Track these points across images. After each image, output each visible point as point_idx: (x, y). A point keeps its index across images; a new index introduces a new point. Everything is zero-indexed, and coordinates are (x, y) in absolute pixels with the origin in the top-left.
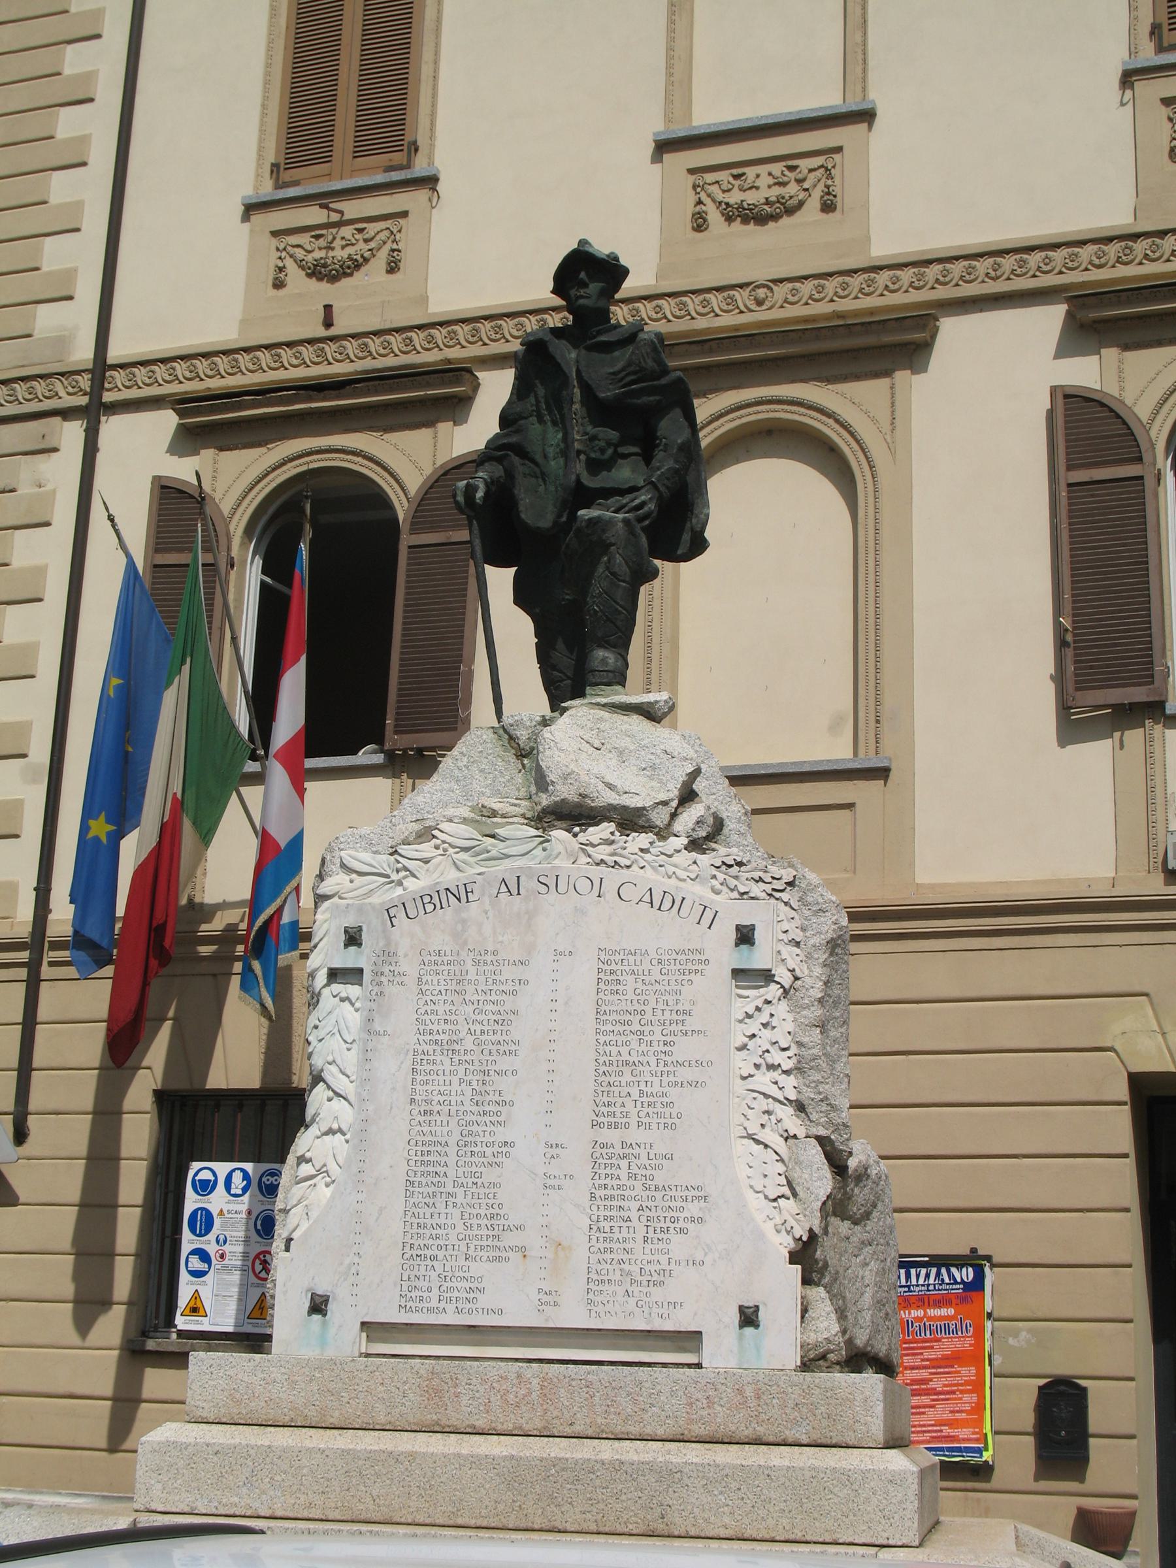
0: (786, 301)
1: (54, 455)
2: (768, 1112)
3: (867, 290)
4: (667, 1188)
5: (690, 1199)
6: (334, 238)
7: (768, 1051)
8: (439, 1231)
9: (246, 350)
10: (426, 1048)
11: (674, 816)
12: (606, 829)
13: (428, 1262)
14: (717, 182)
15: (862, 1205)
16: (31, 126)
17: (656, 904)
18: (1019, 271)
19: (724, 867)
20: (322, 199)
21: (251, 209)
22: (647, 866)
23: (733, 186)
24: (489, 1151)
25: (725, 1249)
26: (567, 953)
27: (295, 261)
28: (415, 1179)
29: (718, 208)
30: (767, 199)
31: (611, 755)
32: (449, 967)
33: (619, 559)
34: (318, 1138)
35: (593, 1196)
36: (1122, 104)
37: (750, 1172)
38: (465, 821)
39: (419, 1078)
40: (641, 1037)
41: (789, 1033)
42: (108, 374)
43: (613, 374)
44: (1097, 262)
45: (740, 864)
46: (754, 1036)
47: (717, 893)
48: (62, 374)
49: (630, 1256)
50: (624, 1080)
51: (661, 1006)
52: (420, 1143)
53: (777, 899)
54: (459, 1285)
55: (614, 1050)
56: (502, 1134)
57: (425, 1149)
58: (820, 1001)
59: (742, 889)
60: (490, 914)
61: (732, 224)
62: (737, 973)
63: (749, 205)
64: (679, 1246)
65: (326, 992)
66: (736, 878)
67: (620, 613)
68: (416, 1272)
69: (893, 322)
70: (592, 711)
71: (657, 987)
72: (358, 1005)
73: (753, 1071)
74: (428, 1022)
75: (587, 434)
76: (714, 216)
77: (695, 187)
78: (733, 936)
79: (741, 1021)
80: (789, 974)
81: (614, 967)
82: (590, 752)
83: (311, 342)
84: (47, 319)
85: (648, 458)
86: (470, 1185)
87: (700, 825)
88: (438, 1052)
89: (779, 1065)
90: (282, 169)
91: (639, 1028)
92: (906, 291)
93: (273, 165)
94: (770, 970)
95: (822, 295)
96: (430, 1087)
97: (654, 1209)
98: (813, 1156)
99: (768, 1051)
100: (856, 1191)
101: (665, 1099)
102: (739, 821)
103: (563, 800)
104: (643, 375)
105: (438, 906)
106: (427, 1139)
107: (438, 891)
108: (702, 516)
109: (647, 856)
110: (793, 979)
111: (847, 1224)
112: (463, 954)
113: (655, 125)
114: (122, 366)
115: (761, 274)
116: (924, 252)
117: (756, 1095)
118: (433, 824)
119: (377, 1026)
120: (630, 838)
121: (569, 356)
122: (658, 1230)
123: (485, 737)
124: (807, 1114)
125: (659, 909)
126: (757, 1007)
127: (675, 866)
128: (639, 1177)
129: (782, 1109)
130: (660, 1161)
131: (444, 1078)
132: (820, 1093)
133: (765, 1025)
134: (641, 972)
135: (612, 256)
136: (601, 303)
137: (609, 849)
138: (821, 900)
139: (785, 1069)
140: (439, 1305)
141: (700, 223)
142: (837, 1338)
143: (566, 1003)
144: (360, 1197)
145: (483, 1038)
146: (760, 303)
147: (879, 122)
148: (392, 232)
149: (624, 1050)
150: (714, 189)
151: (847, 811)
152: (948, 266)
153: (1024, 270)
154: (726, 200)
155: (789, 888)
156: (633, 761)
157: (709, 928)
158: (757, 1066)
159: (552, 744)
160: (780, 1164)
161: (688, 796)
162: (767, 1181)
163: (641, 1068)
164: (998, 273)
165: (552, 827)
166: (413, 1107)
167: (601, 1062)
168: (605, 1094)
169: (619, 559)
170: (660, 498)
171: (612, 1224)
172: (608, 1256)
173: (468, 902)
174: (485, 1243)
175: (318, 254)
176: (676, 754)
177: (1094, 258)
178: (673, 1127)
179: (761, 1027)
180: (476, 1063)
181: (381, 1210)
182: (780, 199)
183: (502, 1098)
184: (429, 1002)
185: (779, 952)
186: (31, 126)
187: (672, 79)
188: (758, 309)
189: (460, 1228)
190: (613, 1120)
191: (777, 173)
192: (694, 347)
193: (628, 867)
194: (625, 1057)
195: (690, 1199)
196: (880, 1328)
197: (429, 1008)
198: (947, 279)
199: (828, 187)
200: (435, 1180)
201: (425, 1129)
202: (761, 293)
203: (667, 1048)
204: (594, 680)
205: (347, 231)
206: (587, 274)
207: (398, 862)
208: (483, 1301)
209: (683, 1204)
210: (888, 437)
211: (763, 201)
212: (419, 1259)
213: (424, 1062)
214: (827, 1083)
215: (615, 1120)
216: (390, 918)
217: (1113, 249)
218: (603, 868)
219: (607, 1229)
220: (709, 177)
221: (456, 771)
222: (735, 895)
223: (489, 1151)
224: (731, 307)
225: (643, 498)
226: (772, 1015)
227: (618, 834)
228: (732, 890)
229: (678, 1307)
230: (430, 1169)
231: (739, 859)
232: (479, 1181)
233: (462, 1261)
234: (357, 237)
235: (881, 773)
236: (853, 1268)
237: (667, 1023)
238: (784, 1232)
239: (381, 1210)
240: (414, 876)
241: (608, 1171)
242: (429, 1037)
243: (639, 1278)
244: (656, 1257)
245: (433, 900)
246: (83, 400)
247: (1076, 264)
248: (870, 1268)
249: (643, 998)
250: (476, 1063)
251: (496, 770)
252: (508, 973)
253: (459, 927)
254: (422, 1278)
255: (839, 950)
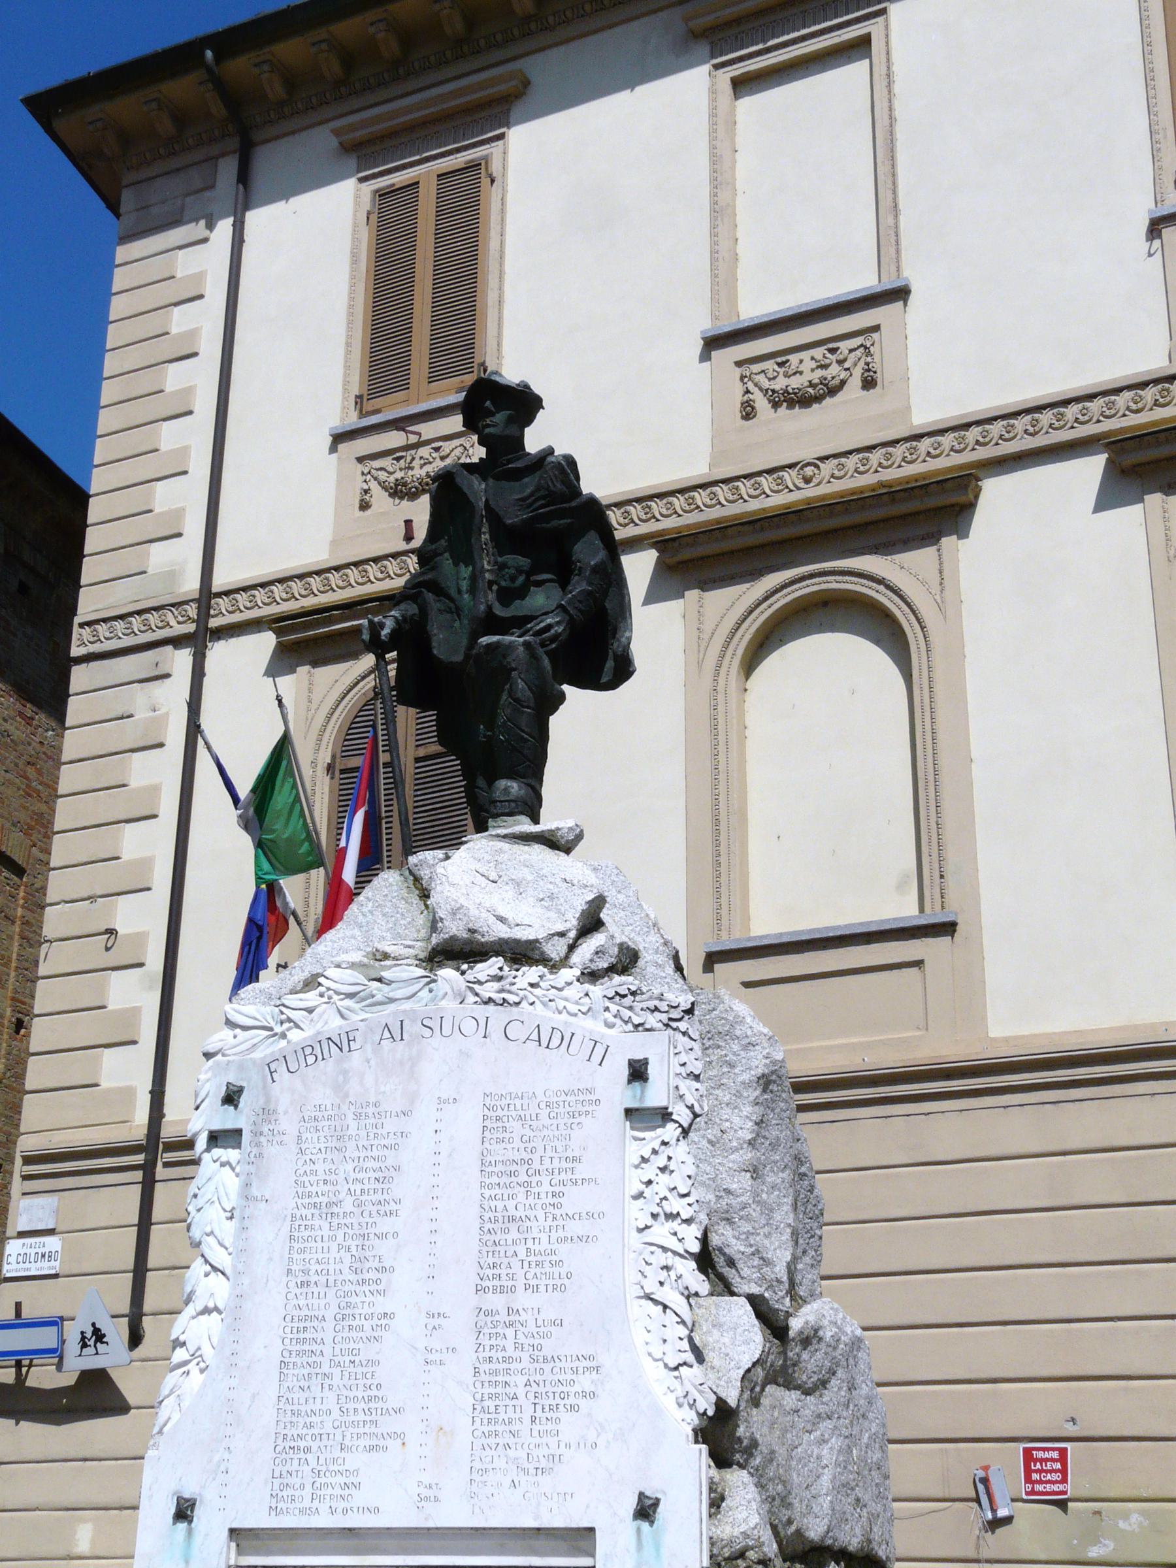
0: (833, 476)
1: (167, 681)
2: (666, 1268)
3: (909, 458)
4: (556, 1359)
5: (581, 1370)
6: (413, 459)
7: (665, 1198)
8: (313, 1419)
9: (337, 569)
10: (304, 1212)
11: (572, 948)
12: (494, 964)
13: (302, 1455)
14: (763, 371)
15: (814, 1372)
16: (143, 383)
17: (544, 1042)
18: (1057, 424)
19: (618, 998)
20: (399, 424)
21: (339, 438)
22: (537, 1002)
23: (778, 373)
24: (367, 1325)
25: (621, 1429)
26: (451, 1101)
27: (379, 483)
28: (289, 1360)
29: (765, 395)
30: (810, 382)
31: (507, 888)
32: (329, 1123)
33: (521, 684)
34: (193, 1318)
35: (477, 1372)
36: (1150, 255)
37: (648, 1337)
38: (353, 966)
39: (296, 1246)
40: (529, 1189)
41: (689, 1177)
42: (213, 602)
43: (523, 500)
44: (1134, 407)
45: (634, 994)
46: (650, 1182)
47: (610, 1026)
48: (173, 605)
49: (517, 1440)
50: (510, 1238)
51: (549, 1153)
52: (296, 1319)
53: (674, 1029)
54: (333, 1480)
55: (500, 1205)
56: (382, 1304)
57: (302, 1325)
58: (751, 1143)
59: (636, 1020)
60: (373, 1063)
61: (779, 410)
62: (629, 1112)
63: (793, 389)
64: (570, 1426)
65: (206, 1157)
66: (630, 1008)
67: (526, 740)
68: (288, 1467)
69: (935, 485)
70: (491, 843)
71: (545, 1132)
72: (238, 1169)
73: (650, 1221)
74: (307, 1184)
75: (496, 563)
76: (761, 403)
77: (742, 378)
78: (625, 1072)
79: (637, 1167)
80: (688, 1111)
81: (500, 1113)
82: (483, 886)
83: (395, 555)
84: (159, 556)
85: (564, 583)
86: (347, 1364)
87: (600, 955)
88: (317, 1216)
89: (678, 1214)
90: (365, 400)
91: (526, 1178)
92: (948, 455)
93: (357, 397)
94: (667, 1108)
95: (867, 467)
96: (307, 1256)
97: (542, 1384)
98: (739, 1317)
99: (665, 1198)
100: (805, 1356)
101: (554, 1258)
102: (657, 952)
103: (451, 937)
104: (552, 497)
105: (320, 1057)
106: (303, 1313)
107: (320, 1042)
108: (623, 639)
109: (537, 991)
110: (692, 1116)
111: (795, 1394)
112: (344, 1107)
113: (704, 324)
114: (227, 593)
115: (808, 454)
116: (962, 416)
117: (653, 1248)
118: (320, 971)
119: (255, 1191)
120: (520, 973)
121: (478, 489)
122: (547, 1409)
123: (391, 880)
124: (737, 1270)
125: (547, 1047)
126: (653, 1149)
127: (566, 999)
128: (526, 1347)
129: (682, 1263)
130: (549, 1328)
131: (323, 1244)
132: (751, 1246)
133: (663, 1170)
134: (528, 1117)
135: (522, 384)
136: (512, 431)
137: (496, 985)
138: (749, 1033)
139: (684, 1217)
140: (312, 1505)
141: (748, 412)
142: (756, 1532)
143: (450, 1155)
144: (234, 1382)
145: (364, 1198)
146: (807, 480)
147: (913, 298)
148: (465, 448)
149: (511, 1205)
150: (761, 378)
151: (915, 969)
152: (987, 427)
153: (1062, 423)
154: (772, 387)
155: (687, 1017)
156: (530, 892)
157: (600, 1065)
158: (654, 1216)
159: (444, 879)
160: (681, 1327)
161: (591, 923)
162: (668, 1347)
163: (528, 1224)
164: (1037, 429)
165: (441, 965)
166: (290, 1278)
167: (486, 1219)
168: (490, 1254)
169: (521, 684)
170: (571, 623)
171: (497, 1402)
172: (492, 1441)
173: (350, 1051)
174: (361, 1430)
175: (399, 475)
176: (575, 882)
177: (1131, 404)
178: (562, 1288)
179: (658, 1171)
180: (356, 1226)
181: (254, 1396)
182: (823, 380)
183: (381, 1265)
184: (308, 1161)
185: (677, 1087)
186: (143, 383)
187: (717, 280)
188: (806, 486)
189: (336, 1413)
190: (498, 1283)
191: (819, 356)
192: (746, 528)
193: (517, 1004)
194: (512, 1212)
195: (581, 1370)
196: (848, 1516)
197: (307, 1168)
198: (987, 440)
199: (867, 364)
200: (310, 1360)
201: (302, 1302)
202: (809, 471)
203: (555, 1200)
204: (495, 811)
205: (424, 452)
206: (493, 403)
207: (282, 1013)
208: (360, 1498)
209: (574, 1377)
210: (938, 598)
211: (807, 384)
212: (292, 1451)
213: (302, 1228)
214: (758, 1234)
215: (502, 1283)
216: (271, 1073)
217: (1150, 394)
218: (491, 1007)
219: (492, 1409)
220: (756, 368)
221: (361, 918)
222: (630, 1027)
223: (367, 1325)
224: (780, 487)
225: (549, 621)
226: (670, 1158)
227: (506, 968)
228: (626, 1022)
229: (568, 1497)
230: (306, 1347)
231: (633, 988)
232: (357, 1359)
233: (337, 1453)
234: (434, 455)
235: (947, 929)
236: (804, 1446)
237: (556, 1171)
238: (686, 1406)
239: (254, 1396)
240: (297, 1026)
241: (493, 1342)
242: (307, 1201)
243: (526, 1465)
244: (544, 1440)
245: (314, 1051)
246: (191, 628)
247: (1113, 412)
248: (830, 1445)
249: (530, 1146)
250: (356, 1226)
251: (398, 913)
252: (390, 1125)
253: (341, 1078)
254: (294, 1474)
255: (773, 1087)
